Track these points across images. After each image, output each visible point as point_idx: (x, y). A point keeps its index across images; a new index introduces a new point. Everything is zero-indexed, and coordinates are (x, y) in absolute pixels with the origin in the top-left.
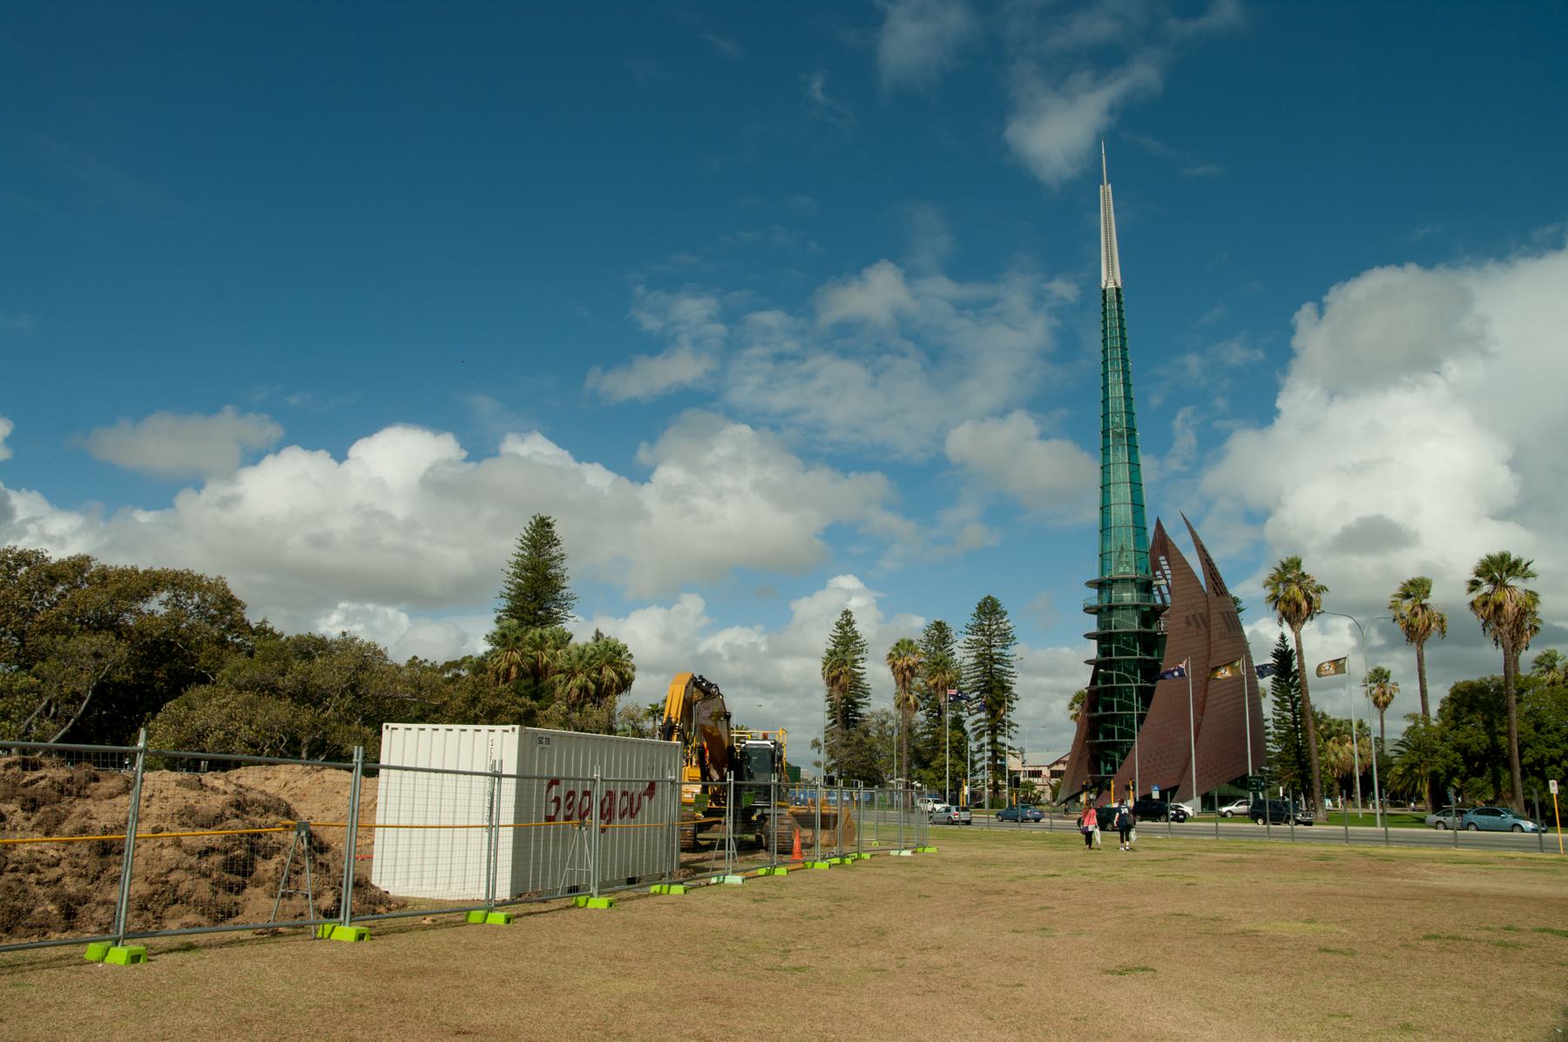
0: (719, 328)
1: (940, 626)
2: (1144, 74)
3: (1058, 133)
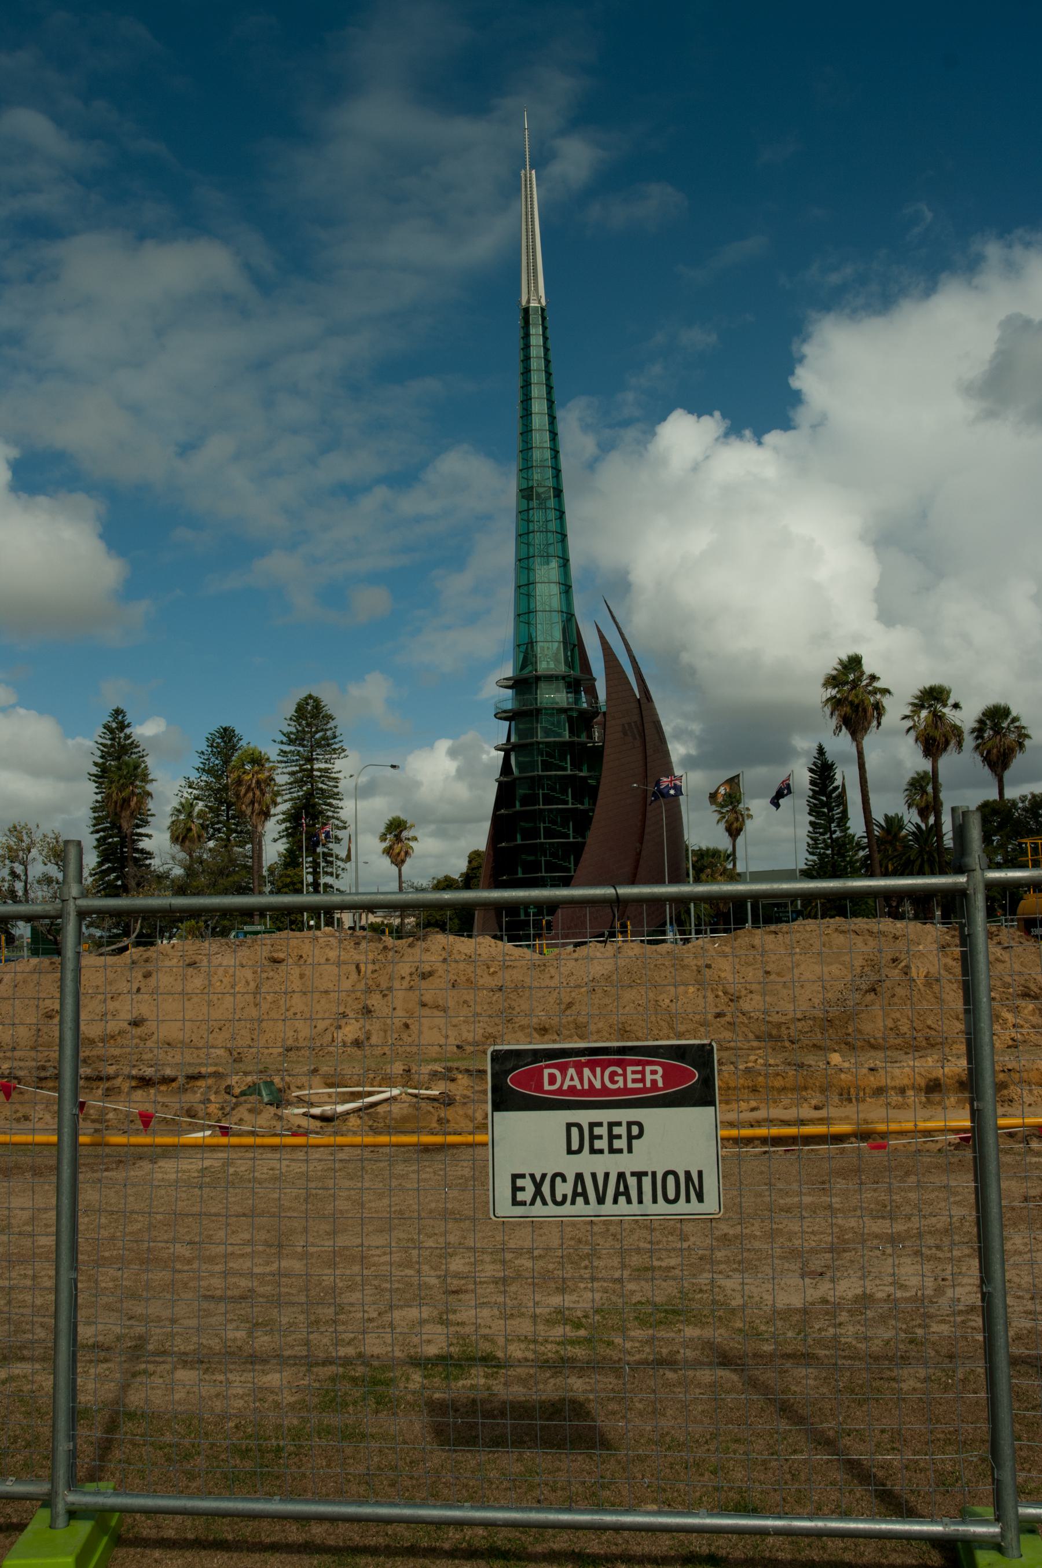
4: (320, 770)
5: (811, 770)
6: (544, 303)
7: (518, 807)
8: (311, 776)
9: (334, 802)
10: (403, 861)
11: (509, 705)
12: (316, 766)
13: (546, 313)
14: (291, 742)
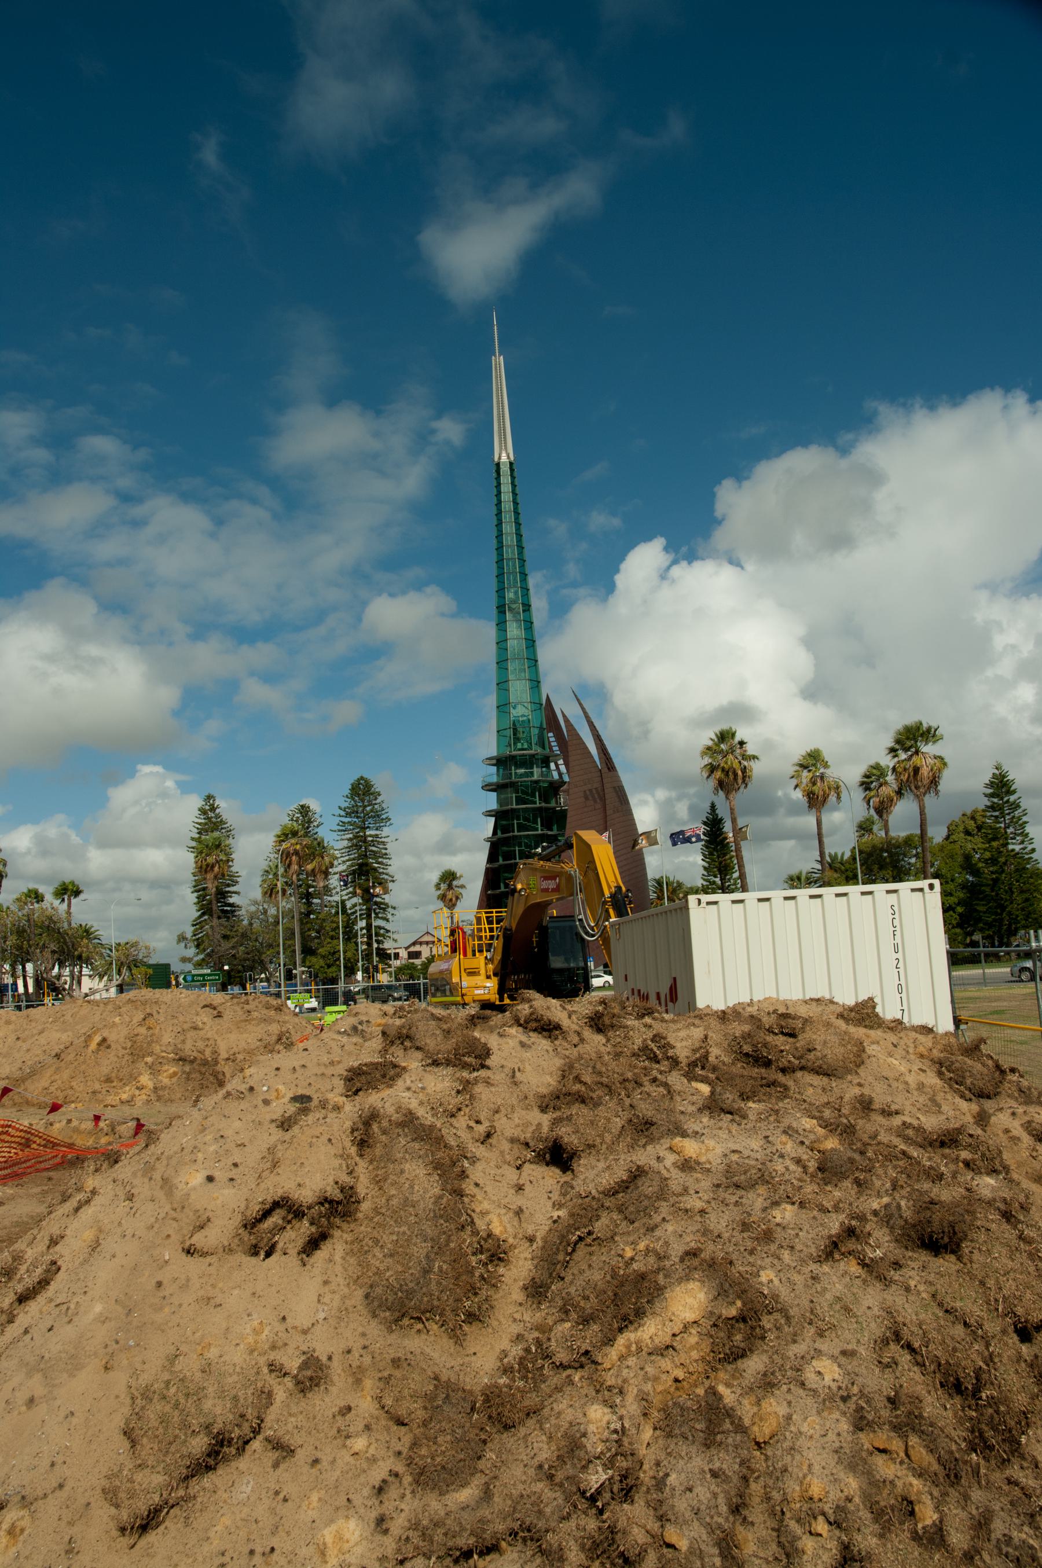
0: (42, 455)
1: (304, 810)
2: (580, 190)
3: (478, 250)
4: (370, 836)
5: (705, 823)
6: (512, 458)
7: (501, 861)
8: (365, 841)
9: (385, 861)
10: (454, 905)
11: (494, 779)
12: (368, 833)
13: (514, 467)
14: (348, 815)
